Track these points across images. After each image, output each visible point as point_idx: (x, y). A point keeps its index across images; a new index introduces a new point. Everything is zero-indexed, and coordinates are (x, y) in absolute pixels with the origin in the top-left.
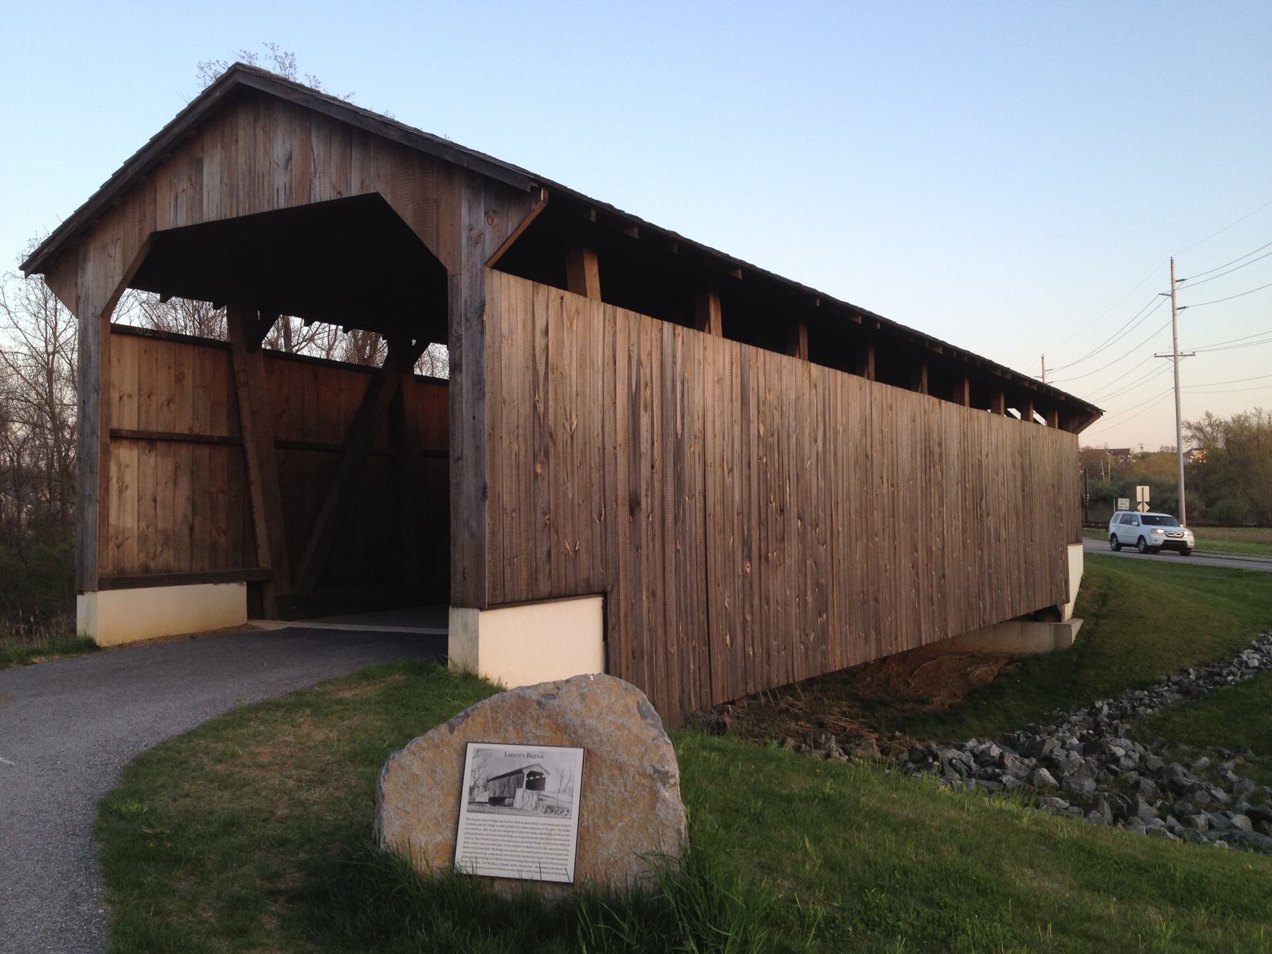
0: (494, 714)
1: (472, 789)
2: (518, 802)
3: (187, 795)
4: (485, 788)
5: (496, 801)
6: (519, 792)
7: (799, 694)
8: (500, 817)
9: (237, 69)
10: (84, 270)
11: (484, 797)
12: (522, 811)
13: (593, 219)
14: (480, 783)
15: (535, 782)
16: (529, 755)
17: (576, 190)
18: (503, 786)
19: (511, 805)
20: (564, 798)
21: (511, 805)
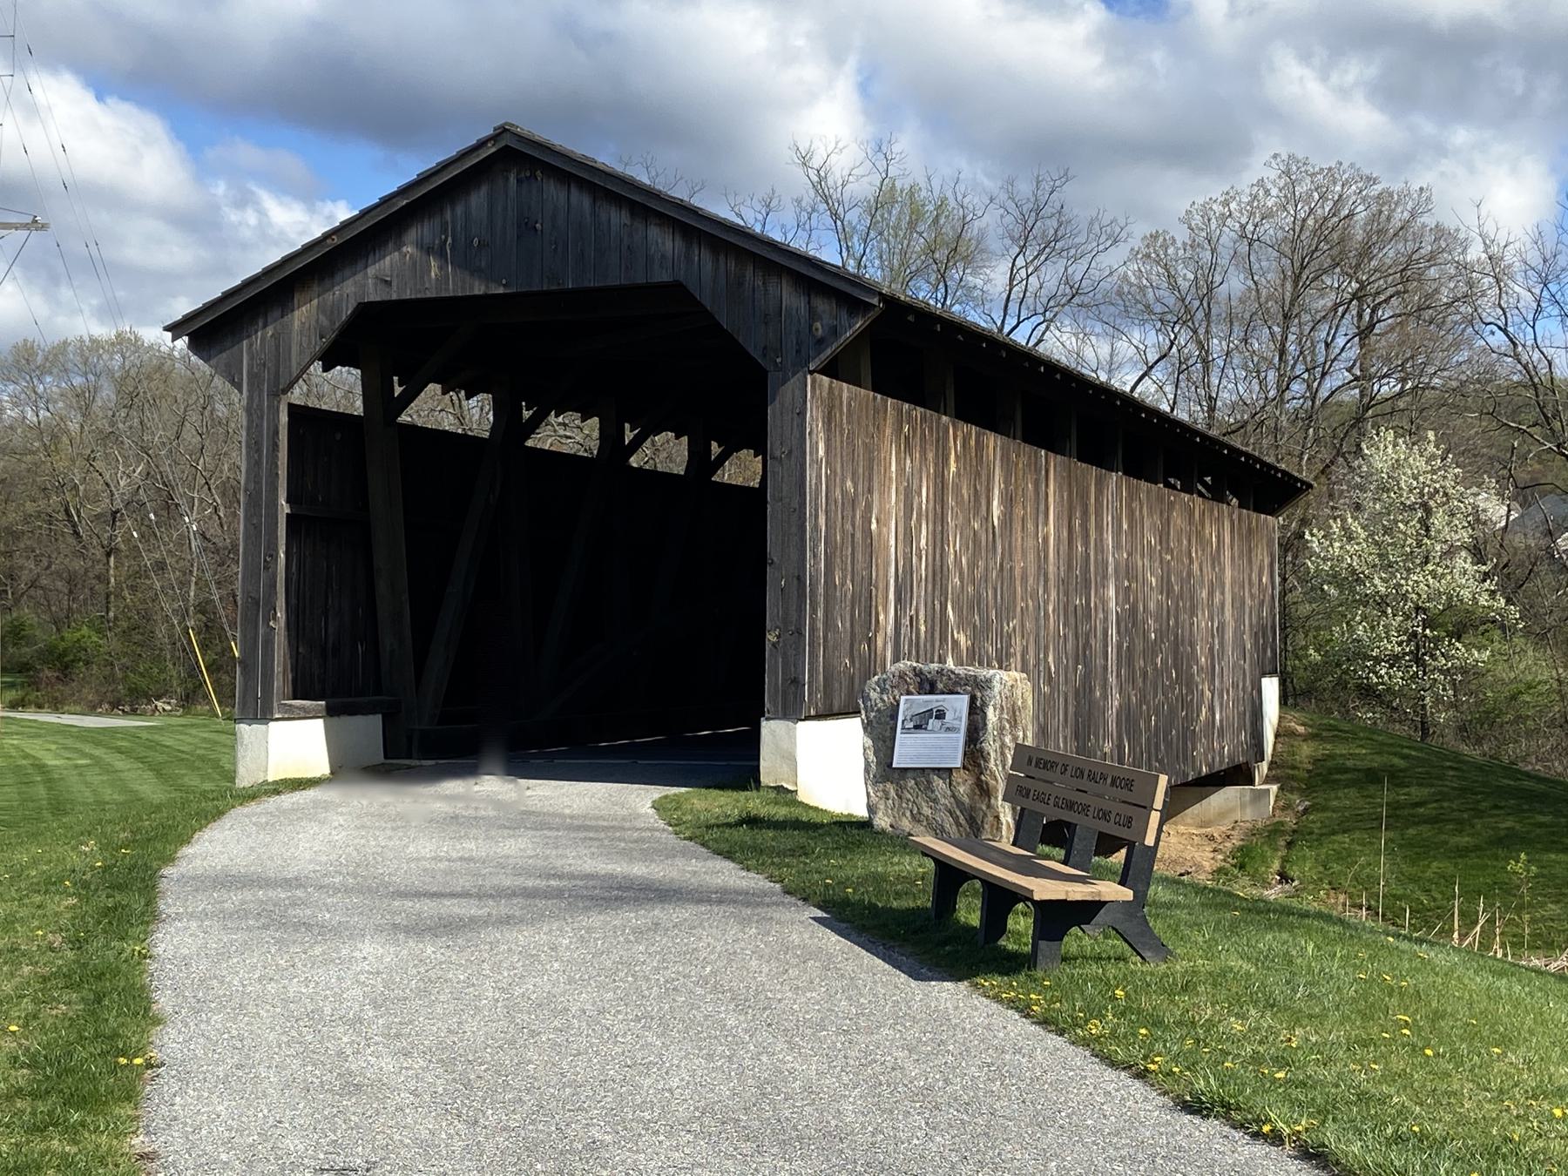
0: (200, 574)
1: (903, 722)
2: (930, 727)
3: (82, 426)
4: (911, 720)
5: (917, 727)
6: (931, 721)
7: (1128, 679)
8: (920, 736)
9: (503, 131)
10: (400, 237)
11: (911, 725)
12: (932, 731)
13: (939, 329)
14: (908, 718)
15: (941, 715)
16: (937, 701)
17: (323, 731)
18: (921, 719)
19: (926, 729)
20: (956, 723)
21: (926, 729)
